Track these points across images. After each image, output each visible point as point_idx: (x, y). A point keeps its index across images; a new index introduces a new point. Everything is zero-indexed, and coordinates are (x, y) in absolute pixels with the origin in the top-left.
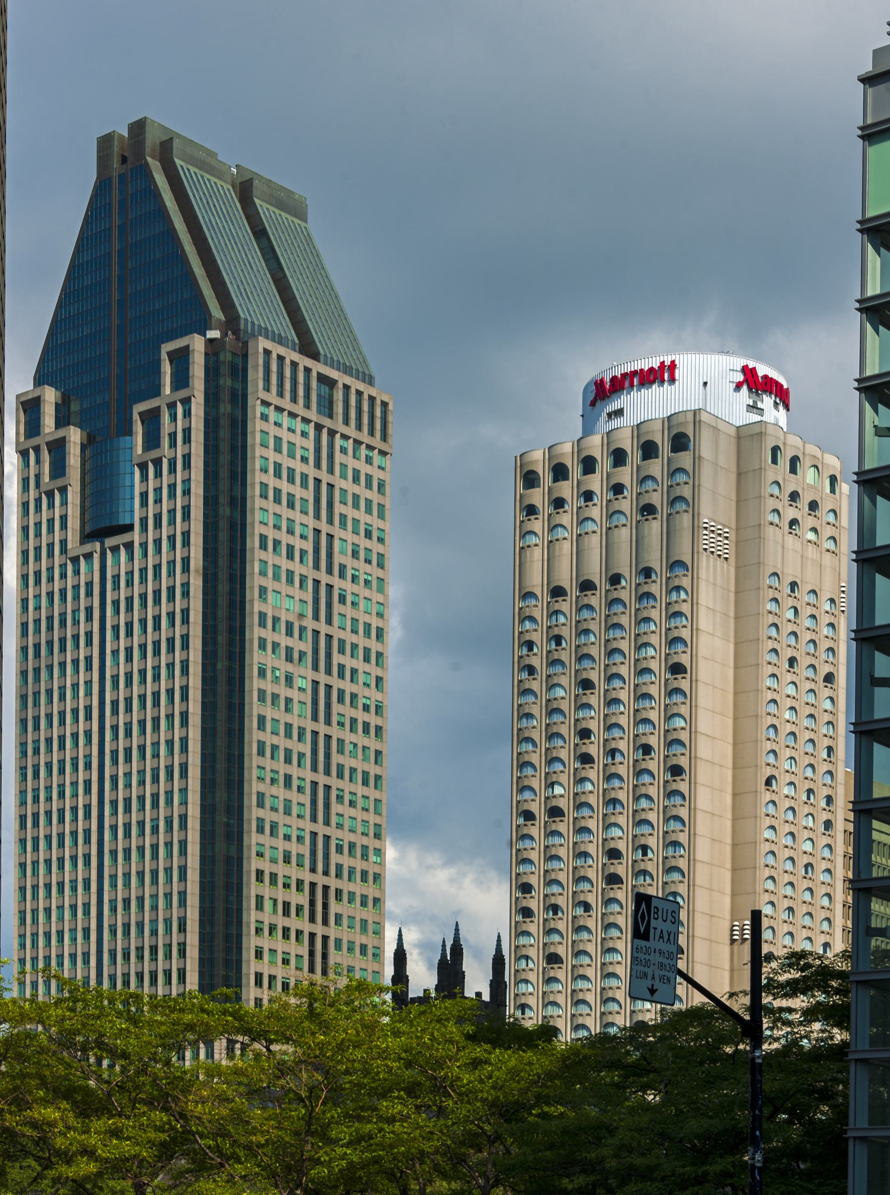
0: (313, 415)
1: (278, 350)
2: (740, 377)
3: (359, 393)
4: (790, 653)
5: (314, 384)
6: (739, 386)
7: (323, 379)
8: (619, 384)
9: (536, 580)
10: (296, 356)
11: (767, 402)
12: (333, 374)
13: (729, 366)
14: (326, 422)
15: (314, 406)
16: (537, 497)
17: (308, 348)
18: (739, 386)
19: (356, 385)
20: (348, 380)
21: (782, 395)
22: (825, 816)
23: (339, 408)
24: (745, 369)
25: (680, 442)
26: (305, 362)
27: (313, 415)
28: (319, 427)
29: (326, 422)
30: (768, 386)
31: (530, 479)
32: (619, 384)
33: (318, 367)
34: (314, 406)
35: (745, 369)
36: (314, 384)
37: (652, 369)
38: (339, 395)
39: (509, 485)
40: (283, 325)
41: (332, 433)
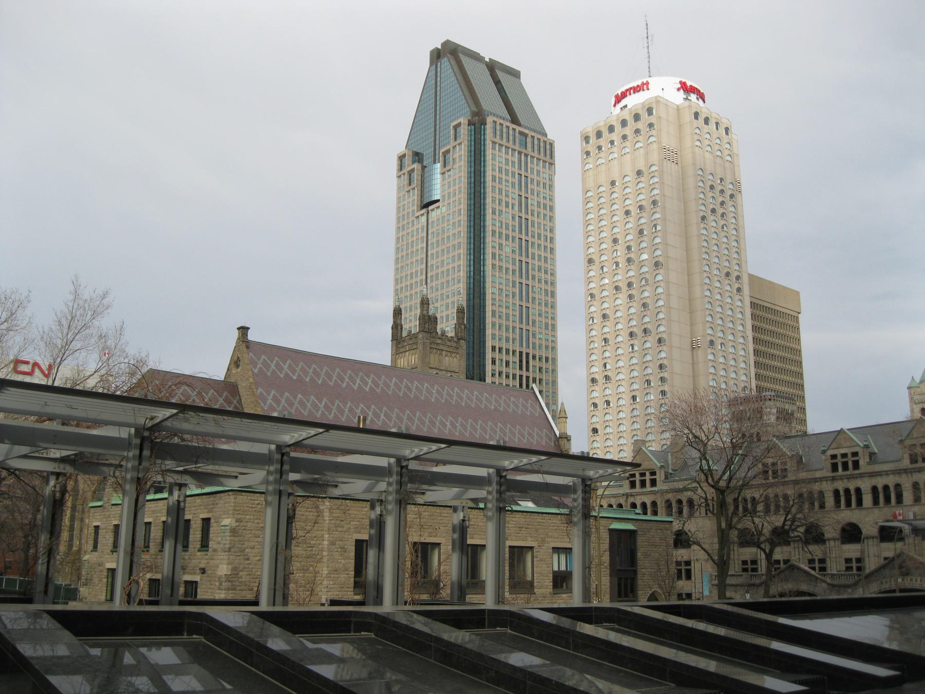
0: (517, 147)
1: (499, 121)
2: (679, 86)
3: (539, 140)
4: (712, 206)
5: (517, 135)
6: (678, 89)
7: (521, 133)
8: (624, 95)
9: (591, 184)
10: (508, 124)
11: (693, 97)
12: (526, 131)
13: (675, 82)
14: (524, 151)
15: (517, 144)
16: (591, 148)
17: (515, 120)
18: (678, 89)
19: (537, 136)
20: (533, 134)
21: (701, 96)
22: (737, 286)
23: (529, 145)
24: (681, 82)
25: (650, 111)
26: (514, 126)
27: (517, 147)
28: (520, 153)
29: (524, 151)
30: (693, 90)
31: (587, 139)
32: (624, 95)
33: (518, 129)
34: (517, 144)
35: (681, 82)
36: (517, 135)
37: (638, 86)
38: (529, 140)
39: (578, 140)
40: (504, 112)
41: (526, 155)
